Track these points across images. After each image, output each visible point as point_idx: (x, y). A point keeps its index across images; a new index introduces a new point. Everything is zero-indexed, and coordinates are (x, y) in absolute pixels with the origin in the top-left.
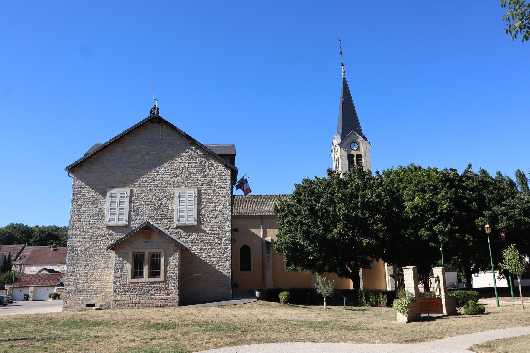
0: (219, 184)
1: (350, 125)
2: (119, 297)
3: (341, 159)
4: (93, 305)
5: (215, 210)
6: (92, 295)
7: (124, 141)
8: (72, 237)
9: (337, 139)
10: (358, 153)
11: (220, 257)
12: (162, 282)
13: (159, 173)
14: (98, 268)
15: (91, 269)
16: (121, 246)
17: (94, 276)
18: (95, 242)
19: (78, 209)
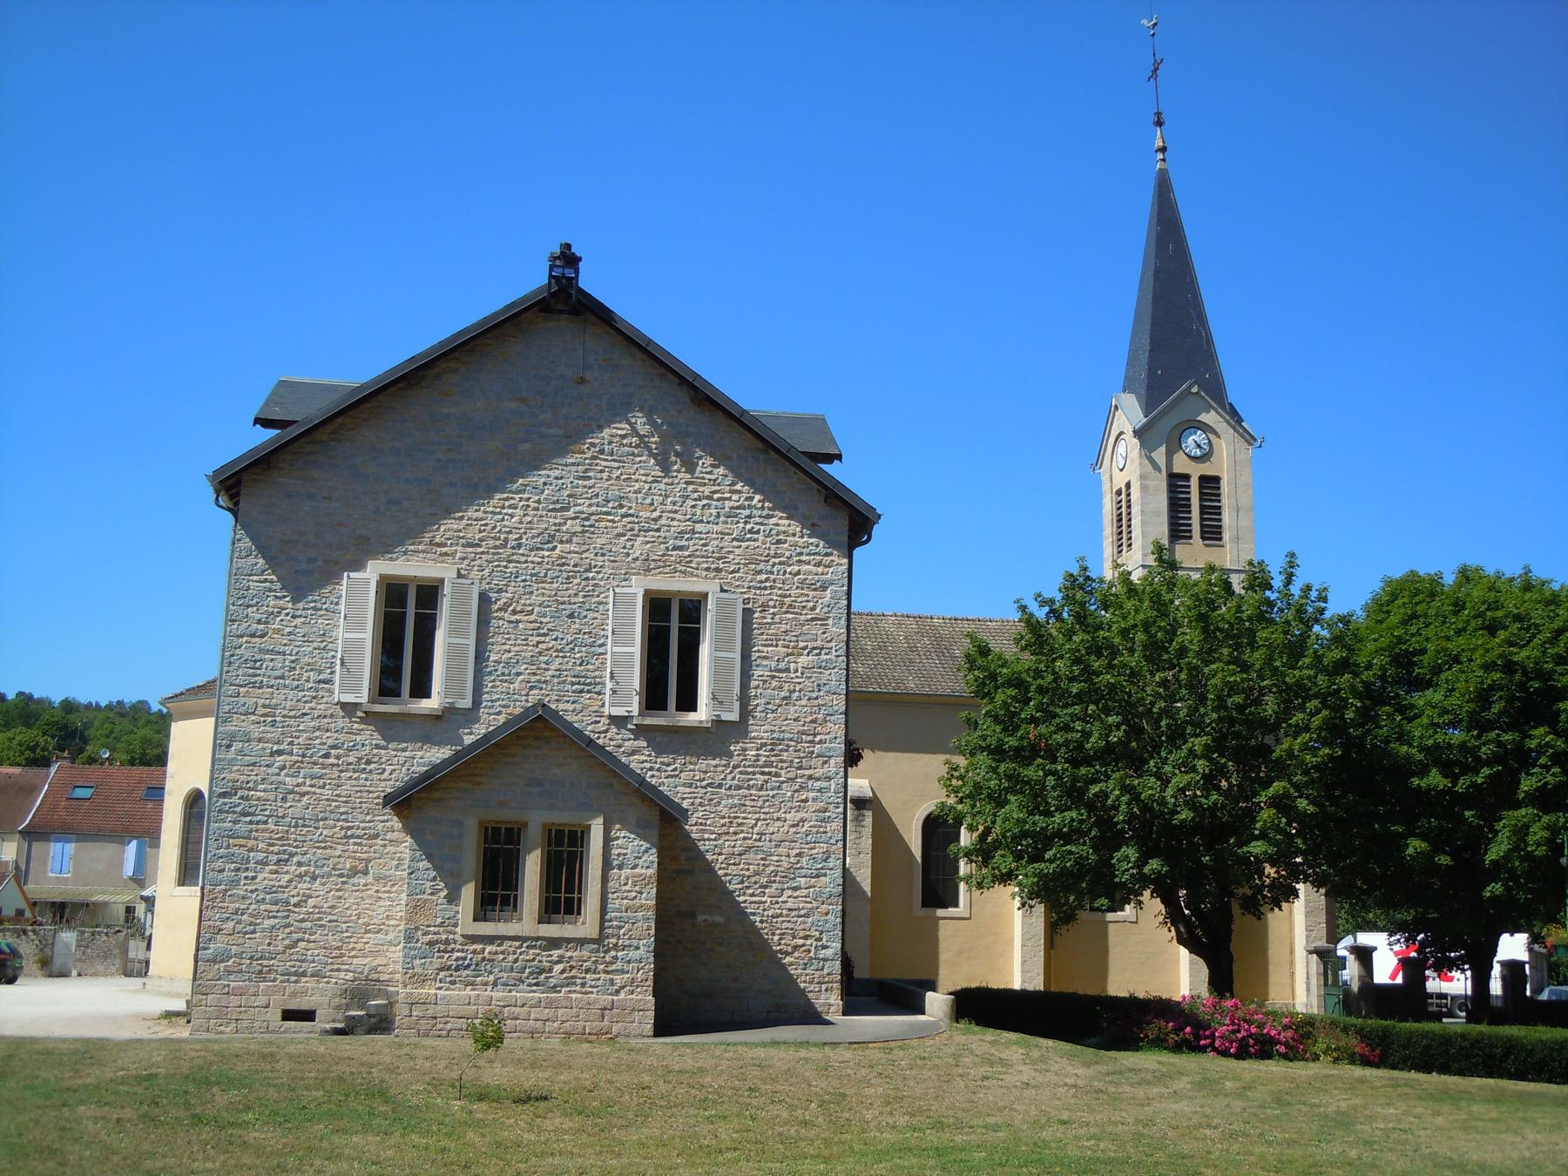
0: (805, 568)
1: (1177, 361)
2: (428, 991)
3: (1144, 489)
4: (308, 1016)
5: (787, 670)
6: (304, 974)
7: (438, 377)
8: (229, 746)
9: (1129, 414)
10: (1208, 469)
11: (799, 855)
12: (593, 941)
13: (570, 514)
14: (330, 875)
15: (300, 876)
16: (436, 795)
17: (311, 902)
18: (316, 770)
19: (253, 636)
